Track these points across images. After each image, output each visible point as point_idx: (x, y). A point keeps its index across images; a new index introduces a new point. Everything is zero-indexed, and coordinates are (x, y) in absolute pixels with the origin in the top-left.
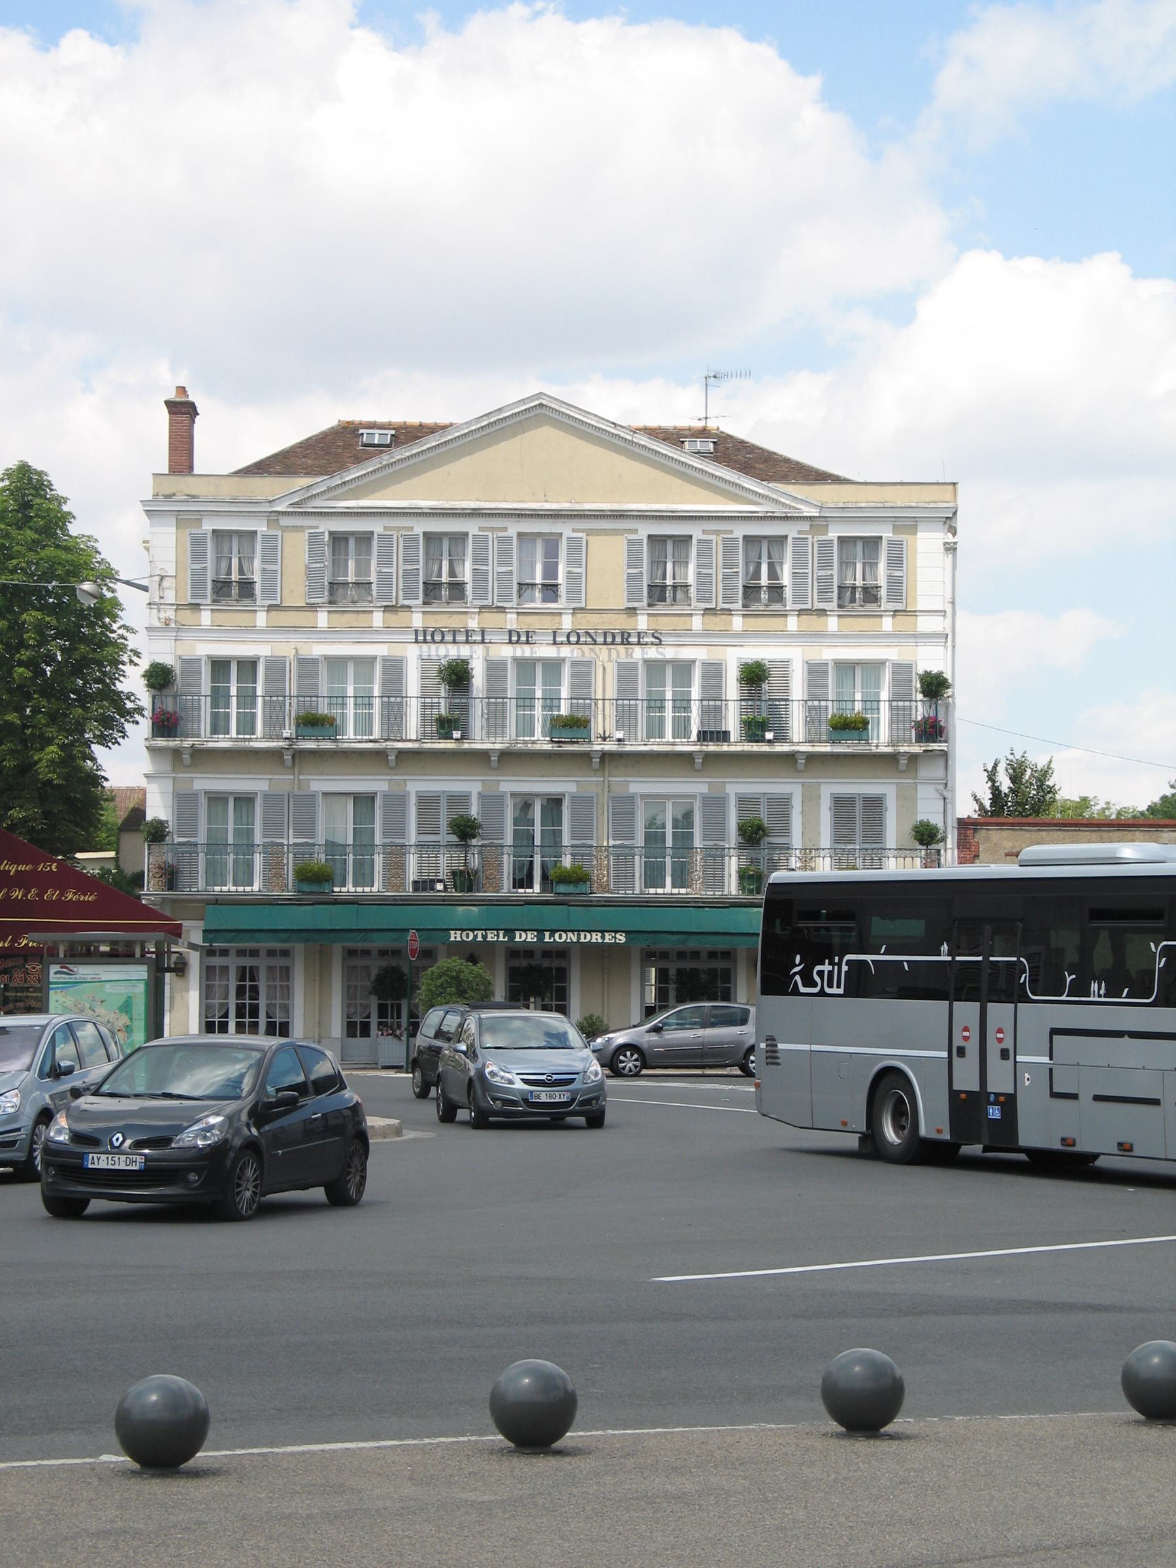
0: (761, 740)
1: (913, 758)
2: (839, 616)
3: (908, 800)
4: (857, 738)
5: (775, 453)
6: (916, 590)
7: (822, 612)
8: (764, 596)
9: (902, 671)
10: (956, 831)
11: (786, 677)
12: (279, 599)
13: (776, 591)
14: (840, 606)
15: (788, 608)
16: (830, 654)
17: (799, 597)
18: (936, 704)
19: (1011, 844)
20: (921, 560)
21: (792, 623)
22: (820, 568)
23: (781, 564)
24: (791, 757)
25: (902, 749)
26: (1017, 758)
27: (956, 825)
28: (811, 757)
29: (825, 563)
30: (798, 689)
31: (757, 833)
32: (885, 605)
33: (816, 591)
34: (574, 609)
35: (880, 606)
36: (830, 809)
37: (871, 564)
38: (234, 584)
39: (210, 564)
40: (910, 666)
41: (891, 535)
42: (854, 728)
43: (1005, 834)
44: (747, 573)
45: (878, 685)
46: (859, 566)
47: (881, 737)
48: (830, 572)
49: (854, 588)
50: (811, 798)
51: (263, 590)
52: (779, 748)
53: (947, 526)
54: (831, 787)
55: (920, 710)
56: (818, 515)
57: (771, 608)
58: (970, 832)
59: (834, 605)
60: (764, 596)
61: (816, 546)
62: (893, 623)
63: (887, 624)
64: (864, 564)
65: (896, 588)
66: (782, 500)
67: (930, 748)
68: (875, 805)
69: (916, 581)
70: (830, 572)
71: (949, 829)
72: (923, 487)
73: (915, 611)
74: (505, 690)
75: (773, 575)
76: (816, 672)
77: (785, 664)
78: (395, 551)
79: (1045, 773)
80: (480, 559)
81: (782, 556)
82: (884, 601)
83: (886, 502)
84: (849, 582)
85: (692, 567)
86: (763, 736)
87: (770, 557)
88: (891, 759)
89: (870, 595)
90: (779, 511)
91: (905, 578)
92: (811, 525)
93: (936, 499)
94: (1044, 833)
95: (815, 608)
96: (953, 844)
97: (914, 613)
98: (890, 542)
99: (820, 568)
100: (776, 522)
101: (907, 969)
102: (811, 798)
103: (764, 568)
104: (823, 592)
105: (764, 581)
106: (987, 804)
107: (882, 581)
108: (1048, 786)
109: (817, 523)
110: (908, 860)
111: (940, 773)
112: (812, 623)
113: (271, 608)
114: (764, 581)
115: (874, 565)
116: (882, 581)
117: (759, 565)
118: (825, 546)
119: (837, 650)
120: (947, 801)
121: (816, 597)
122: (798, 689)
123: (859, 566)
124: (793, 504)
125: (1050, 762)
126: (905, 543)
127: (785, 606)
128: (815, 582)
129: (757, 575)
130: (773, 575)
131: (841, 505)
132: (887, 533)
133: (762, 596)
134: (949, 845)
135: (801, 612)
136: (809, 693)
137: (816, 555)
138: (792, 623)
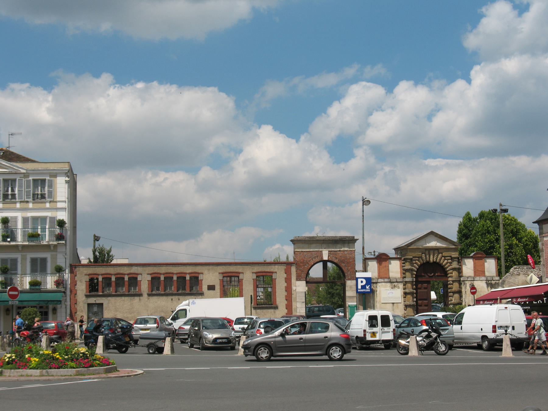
0: (7, 241)
1: (55, 246)
2: (33, 203)
3: (54, 258)
4: (36, 240)
5: (21, 155)
6: (57, 195)
7: (27, 202)
8: (10, 197)
9: (52, 219)
10: (69, 268)
11: (16, 222)
12: (24, 199)
13: (13, 196)
14: (33, 200)
15: (17, 201)
16: (30, 214)
17: (20, 197)
18: (63, 229)
19: (86, 272)
20: (58, 186)
21: (18, 205)
22: (27, 188)
23: (15, 187)
24: (17, 246)
25: (51, 243)
26: (101, 247)
27: (69, 266)
28: (23, 246)
29: (28, 186)
30: (20, 225)
31: (5, 270)
32: (47, 199)
33: (25, 195)
34: (50, 201)
35: (46, 200)
36: (30, 262)
37: (43, 187)
38: (10, 195)
39: (31, 189)
40: (55, 218)
41: (49, 178)
42: (35, 237)
43: (84, 268)
44: (4, 190)
45: (46, 224)
46: (39, 188)
47: (47, 239)
48: (30, 189)
49: (38, 194)
50: (24, 259)
51: (19, 196)
52: (13, 243)
53: (66, 175)
54: (30, 256)
55: (58, 231)
56: (26, 172)
57: (12, 201)
58: (74, 268)
59: (31, 200)
60: (10, 197)
61: (25, 181)
62: (50, 205)
63: (48, 205)
64: (41, 187)
65: (51, 193)
66: (15, 168)
67: (59, 243)
68: (44, 261)
69: (56, 192)
70: (30, 189)
71: (67, 267)
72: (65, 163)
73: (56, 201)
74: (29, 227)
75: (13, 190)
76: (25, 220)
77: (16, 218)
78: (25, 186)
79: (110, 251)
80: (20, 186)
81: (15, 185)
82: (47, 198)
83: (47, 168)
84: (36, 193)
85: (46, 188)
86: (7, 240)
87: (12, 185)
88: (48, 246)
89: (43, 196)
90: (14, 171)
91: (53, 191)
92: (24, 175)
93: (63, 167)
94: (96, 268)
95: (25, 200)
96: (68, 272)
97: (56, 202)
98: (49, 180)
99: (27, 188)
100: (12, 175)
101: (545, 302)
102: (24, 259)
103: (10, 189)
104: (28, 196)
105: (10, 192)
106: (92, 260)
107: (46, 192)
108: (110, 255)
109: (26, 175)
110: (53, 277)
111: (64, 250)
112: (24, 205)
113: (50, 202)
114: (10, 192)
115: (44, 187)
116: (46, 192)
117: (8, 188)
118: (28, 182)
119: (32, 213)
120: (66, 259)
121: (25, 197)
122: (20, 225)
123: (39, 188)
124: (18, 169)
125: (111, 248)
126: (53, 181)
127: (16, 200)
128: (25, 193)
129: (8, 191)
130: (13, 190)
131: (33, 169)
132: (48, 178)
133: (9, 197)
134: (67, 272)
135: (21, 202)
136: (23, 227)
137: (25, 184)
138: (18, 205)
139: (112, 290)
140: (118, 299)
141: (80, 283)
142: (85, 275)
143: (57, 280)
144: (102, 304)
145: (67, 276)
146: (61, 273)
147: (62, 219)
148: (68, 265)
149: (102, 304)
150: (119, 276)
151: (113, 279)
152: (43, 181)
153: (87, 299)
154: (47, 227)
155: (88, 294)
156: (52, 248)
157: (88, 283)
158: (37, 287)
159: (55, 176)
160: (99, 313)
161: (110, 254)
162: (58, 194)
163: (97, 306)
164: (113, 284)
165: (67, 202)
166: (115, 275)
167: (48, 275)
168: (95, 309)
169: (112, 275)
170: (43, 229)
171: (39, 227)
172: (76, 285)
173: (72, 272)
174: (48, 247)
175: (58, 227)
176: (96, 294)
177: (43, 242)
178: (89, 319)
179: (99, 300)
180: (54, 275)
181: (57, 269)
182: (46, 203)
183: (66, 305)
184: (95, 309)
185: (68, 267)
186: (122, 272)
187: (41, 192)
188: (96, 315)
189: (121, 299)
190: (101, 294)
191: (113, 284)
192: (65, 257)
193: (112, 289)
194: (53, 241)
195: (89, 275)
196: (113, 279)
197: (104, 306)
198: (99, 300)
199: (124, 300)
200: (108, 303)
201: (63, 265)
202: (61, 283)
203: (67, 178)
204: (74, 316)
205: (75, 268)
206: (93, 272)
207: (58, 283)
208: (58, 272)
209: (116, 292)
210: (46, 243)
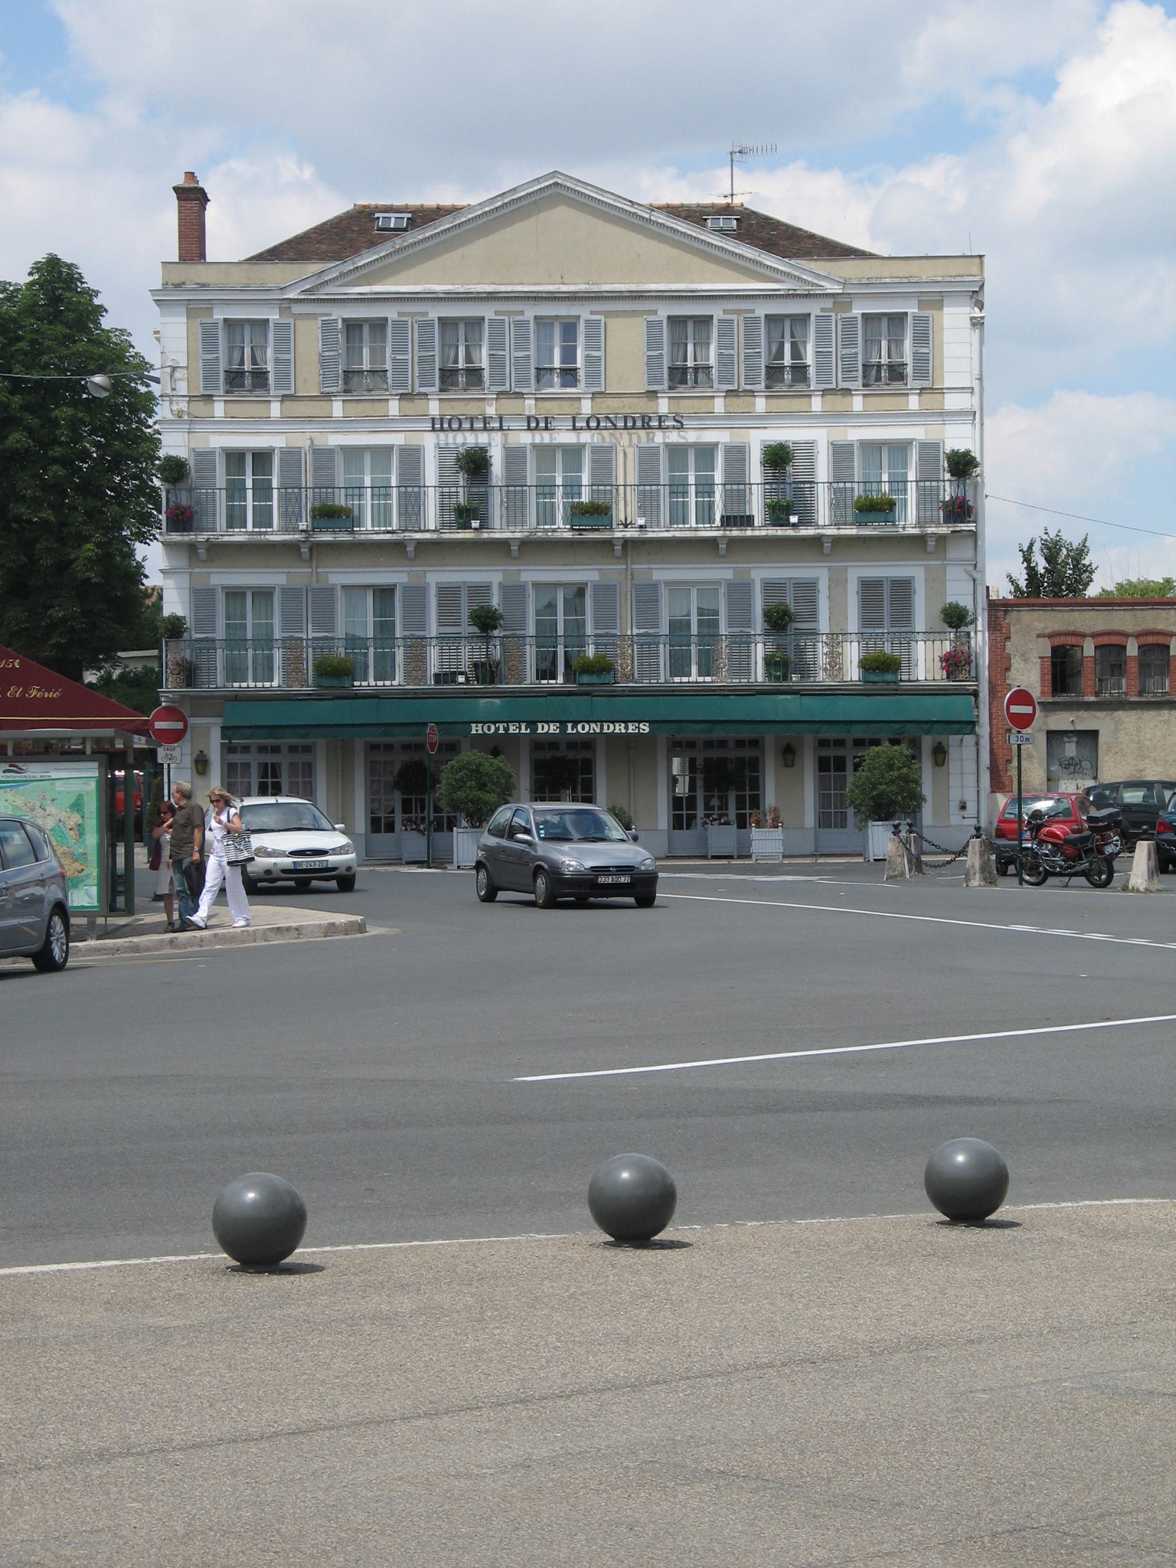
1: (941, 539)
3: (937, 582)
9: (929, 450)
10: (986, 613)
20: (947, 336)
25: (930, 530)
34: (921, 389)
36: (857, 593)
37: (896, 342)
43: (1036, 614)
45: (905, 465)
46: (884, 344)
53: (974, 300)
55: (948, 491)
63: (914, 402)
67: (958, 529)
71: (979, 611)
73: (942, 389)
85: (908, 344)
94: (1076, 614)
97: (941, 391)
98: (915, 318)
107: (908, 358)
110: (937, 643)
111: (969, 554)
116: (908, 358)
123: (884, 344)
125: (1086, 540)
134: (980, 628)
139: (1126, 686)
140: (1149, 715)
141: (1022, 663)
142: (1039, 636)
143: (949, 653)
144: (1094, 734)
145: (980, 639)
146: (963, 629)
147: (962, 450)
148: (982, 603)
149: (1094, 734)
150: (1150, 640)
151: (1132, 650)
152: (898, 320)
153: (1046, 717)
154: (912, 476)
155: (1051, 699)
156: (931, 543)
157: (1048, 664)
158: (889, 677)
159: (938, 304)
160: (1083, 764)
161: (1083, 562)
162: (948, 365)
163: (1075, 739)
164: (1133, 667)
165: (977, 391)
166: (1138, 635)
167: (921, 636)
168: (1071, 749)
169: (1126, 635)
170: (899, 483)
171: (885, 477)
172: (1008, 669)
173: (994, 626)
174: (918, 542)
175: (948, 476)
176: (1074, 699)
177: (904, 528)
178: (1051, 783)
179: (1086, 721)
180: (942, 636)
181: (951, 618)
182: (907, 394)
183: (977, 736)
184: (1071, 749)
185: (983, 609)
186: (1160, 626)
187: (889, 358)
188: (1072, 768)
189: (1160, 718)
190: (1092, 699)
191: (1133, 667)
192: (970, 575)
193: (1128, 685)
194: (938, 525)
195: (1051, 636)
196: (1132, 650)
197: (1102, 739)
198: (1086, 721)
199: (1169, 721)
200: (1117, 730)
201: (966, 602)
202: (963, 663)
203: (977, 309)
204: (1002, 773)
205: (1006, 612)
206: (1063, 628)
207: (955, 663)
208: (953, 627)
209: (1141, 693)
210: (916, 531)
